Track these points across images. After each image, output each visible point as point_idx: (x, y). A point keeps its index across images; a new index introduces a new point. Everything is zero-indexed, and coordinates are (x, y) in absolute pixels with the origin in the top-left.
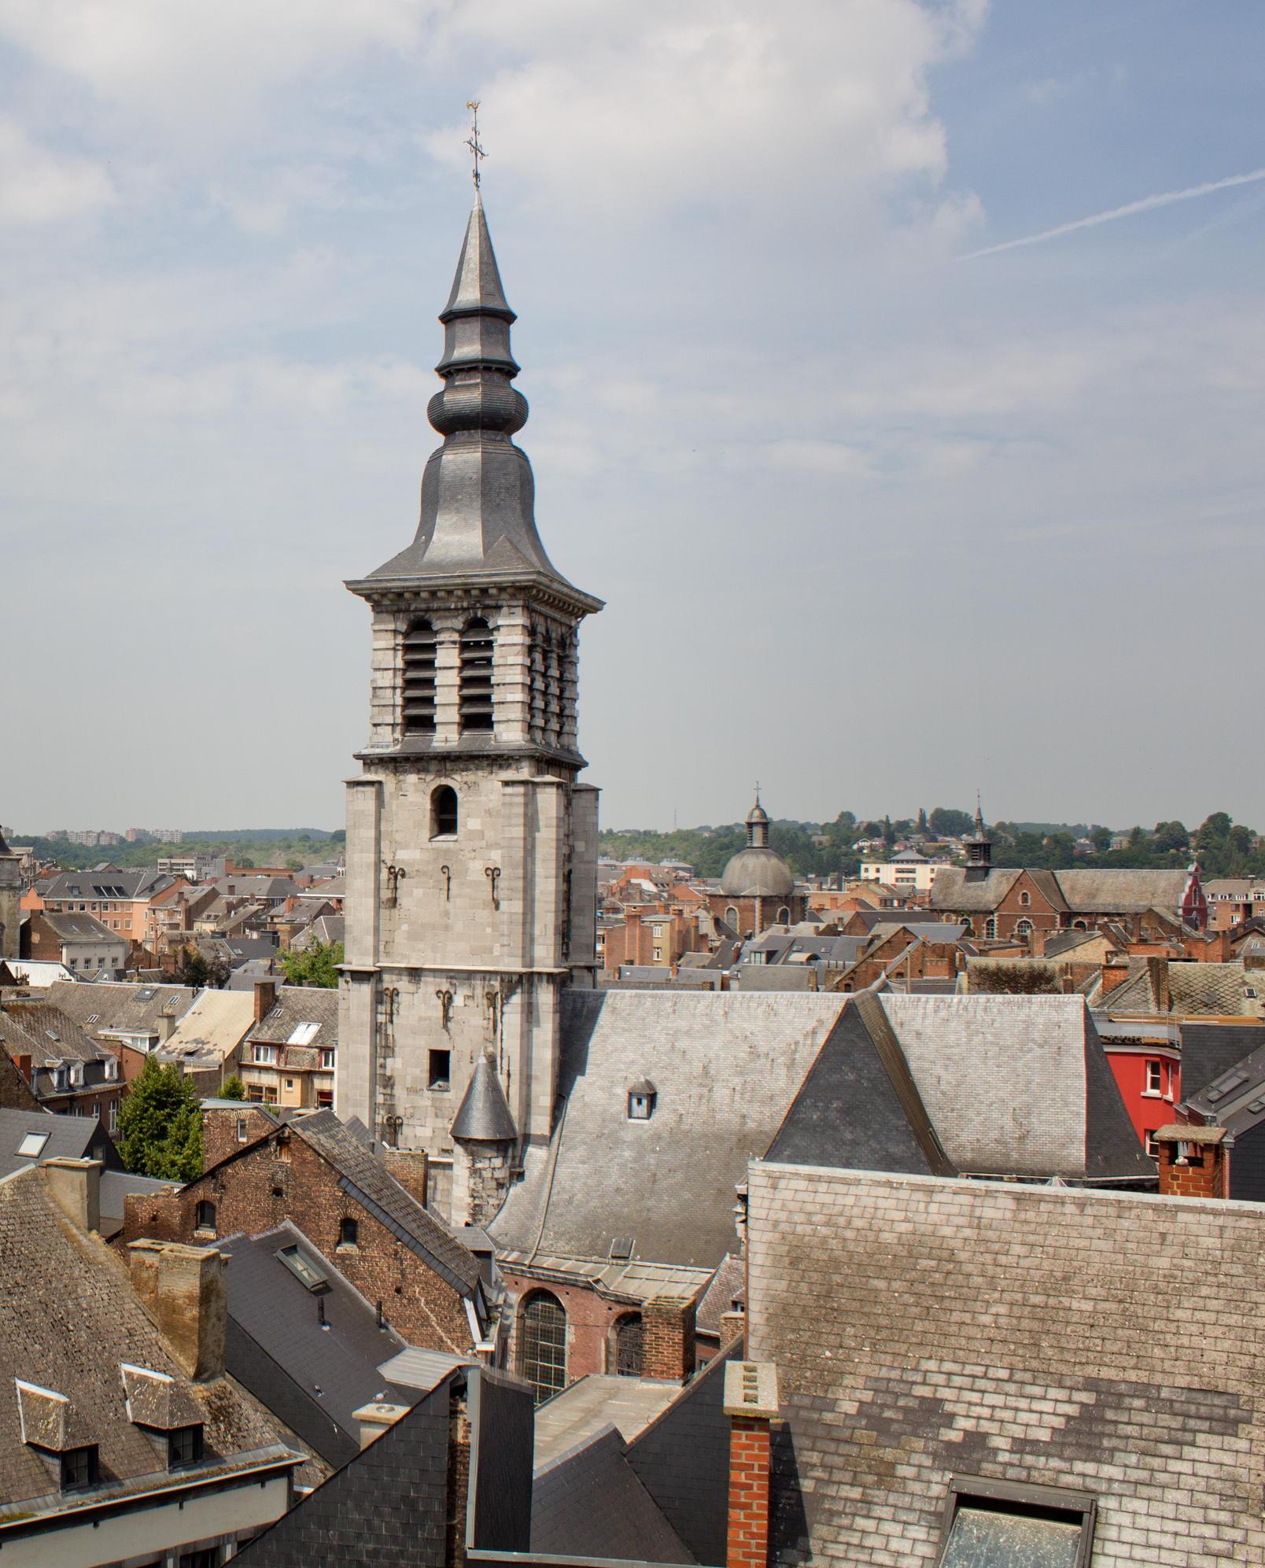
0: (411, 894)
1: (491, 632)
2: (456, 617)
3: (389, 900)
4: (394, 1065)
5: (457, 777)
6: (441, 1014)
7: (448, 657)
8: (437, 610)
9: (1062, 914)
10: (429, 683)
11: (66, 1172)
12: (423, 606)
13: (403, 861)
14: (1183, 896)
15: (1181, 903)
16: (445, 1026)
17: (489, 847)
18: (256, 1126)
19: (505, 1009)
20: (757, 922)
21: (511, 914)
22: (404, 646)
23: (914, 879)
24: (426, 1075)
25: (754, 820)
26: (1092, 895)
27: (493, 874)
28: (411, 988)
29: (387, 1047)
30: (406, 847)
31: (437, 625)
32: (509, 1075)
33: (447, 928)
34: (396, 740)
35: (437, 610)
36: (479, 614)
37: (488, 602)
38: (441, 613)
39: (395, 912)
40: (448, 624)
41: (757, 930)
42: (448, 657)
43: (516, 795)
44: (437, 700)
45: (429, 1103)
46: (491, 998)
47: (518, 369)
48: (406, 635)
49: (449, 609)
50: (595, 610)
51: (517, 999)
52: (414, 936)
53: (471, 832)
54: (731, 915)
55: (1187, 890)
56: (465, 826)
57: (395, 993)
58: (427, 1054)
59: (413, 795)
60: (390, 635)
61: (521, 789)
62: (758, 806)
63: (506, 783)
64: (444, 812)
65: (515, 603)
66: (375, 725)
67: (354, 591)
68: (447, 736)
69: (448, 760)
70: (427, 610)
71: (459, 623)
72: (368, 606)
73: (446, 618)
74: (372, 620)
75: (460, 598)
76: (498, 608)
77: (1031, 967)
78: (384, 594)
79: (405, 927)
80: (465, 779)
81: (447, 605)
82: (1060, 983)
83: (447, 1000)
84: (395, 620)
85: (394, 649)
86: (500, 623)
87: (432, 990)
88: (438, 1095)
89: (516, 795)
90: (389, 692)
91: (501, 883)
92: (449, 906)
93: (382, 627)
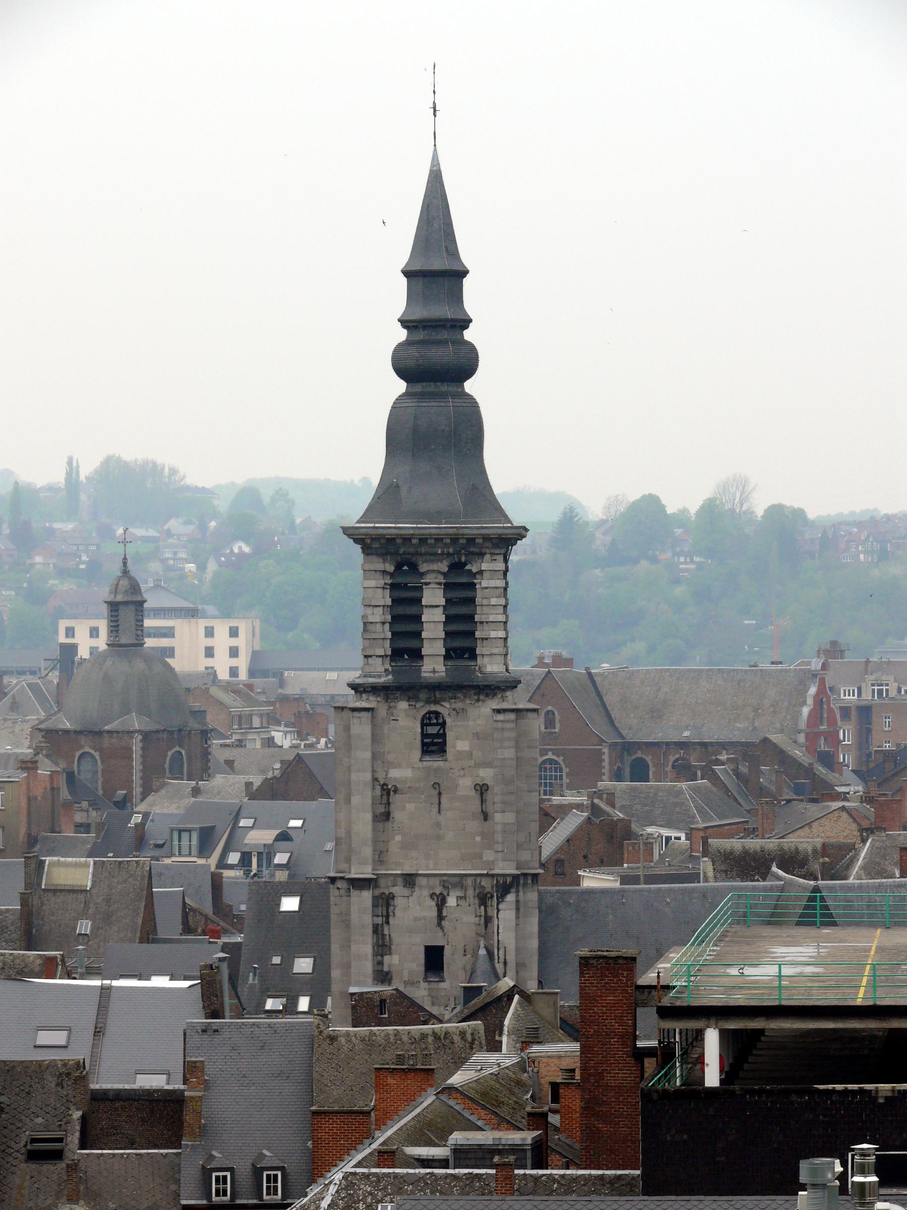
0: (405, 811)
1: (474, 575)
2: (441, 561)
3: (382, 814)
4: (391, 961)
5: (447, 705)
6: (434, 913)
7: (433, 596)
8: (426, 554)
9: (612, 746)
10: (417, 619)
11: (544, 996)
12: (412, 550)
13: (396, 779)
14: (806, 711)
15: (802, 725)
16: (439, 925)
17: (478, 765)
18: (396, 1004)
19: (500, 906)
20: (136, 777)
21: (504, 824)
22: (391, 585)
23: (170, 652)
24: (423, 969)
25: (119, 598)
26: (656, 713)
27: (482, 789)
28: (406, 892)
29: (384, 945)
30: (398, 766)
31: (423, 568)
32: (505, 963)
33: (439, 838)
34: (386, 670)
35: (421, 555)
36: (463, 559)
37: (472, 549)
38: (428, 557)
39: (389, 825)
40: (435, 567)
41: (137, 790)
42: (433, 596)
43: (508, 721)
44: (424, 635)
45: (426, 993)
46: (483, 899)
47: (471, 321)
48: (392, 575)
49: (436, 554)
50: (521, 537)
51: (510, 898)
52: (405, 846)
53: (460, 752)
54: (87, 765)
55: (810, 701)
56: (454, 747)
57: (392, 897)
58: (422, 949)
59: (406, 720)
60: (378, 575)
61: (512, 716)
62: (125, 572)
63: (499, 711)
64: (434, 744)
65: (497, 551)
66: (366, 657)
67: (349, 536)
68: (434, 665)
69: (437, 690)
70: (417, 554)
71: (444, 567)
72: (358, 548)
73: (432, 561)
74: (362, 561)
75: (447, 546)
76: (482, 555)
77: (782, 849)
78: (376, 538)
79: (398, 838)
80: (454, 706)
81: (434, 550)
82: (816, 867)
83: (441, 902)
84: (385, 561)
85: (383, 588)
86: (484, 566)
87: (426, 893)
88: (434, 985)
89: (508, 721)
90: (379, 626)
91: (488, 796)
92: (441, 818)
93: (372, 568)
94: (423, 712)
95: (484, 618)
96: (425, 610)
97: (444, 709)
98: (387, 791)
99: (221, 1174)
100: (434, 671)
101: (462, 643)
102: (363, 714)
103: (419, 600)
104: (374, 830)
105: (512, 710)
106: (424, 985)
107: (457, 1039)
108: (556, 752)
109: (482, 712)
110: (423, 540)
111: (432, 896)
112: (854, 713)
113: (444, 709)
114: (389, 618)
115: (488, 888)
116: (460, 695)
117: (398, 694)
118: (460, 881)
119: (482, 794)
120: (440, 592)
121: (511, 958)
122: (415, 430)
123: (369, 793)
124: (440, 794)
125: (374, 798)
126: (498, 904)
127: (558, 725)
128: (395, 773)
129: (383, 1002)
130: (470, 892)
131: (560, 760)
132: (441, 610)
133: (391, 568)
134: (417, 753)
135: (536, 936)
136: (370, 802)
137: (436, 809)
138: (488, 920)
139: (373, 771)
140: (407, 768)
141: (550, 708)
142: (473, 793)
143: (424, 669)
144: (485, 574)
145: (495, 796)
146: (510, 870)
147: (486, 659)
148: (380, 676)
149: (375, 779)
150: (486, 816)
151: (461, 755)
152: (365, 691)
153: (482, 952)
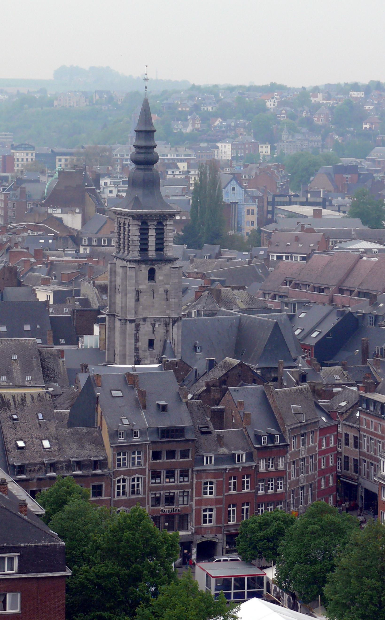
0: (143, 298)
1: (164, 226)
4: (139, 344)
5: (156, 265)
6: (151, 329)
7: (152, 232)
16: (153, 332)
27: (166, 291)
28: (143, 323)
31: (149, 224)
33: (153, 306)
42: (152, 232)
46: (166, 325)
51: (176, 325)
59: (144, 270)
64: (152, 275)
68: (152, 253)
71: (155, 223)
76: (167, 220)
79: (141, 307)
87: (149, 323)
91: (168, 293)
97: (155, 267)
98: (138, 292)
99: (264, 437)
101: (160, 248)
103: (148, 234)
105: (177, 268)
109: (167, 268)
110: (151, 215)
113: (155, 267)
115: (168, 321)
116: (160, 263)
118: (159, 320)
119: (166, 293)
122: (144, 180)
128: (141, 287)
130: (162, 323)
132: (154, 236)
133: (140, 224)
138: (167, 331)
147: (167, 252)
148: (137, 257)
151: (161, 281)
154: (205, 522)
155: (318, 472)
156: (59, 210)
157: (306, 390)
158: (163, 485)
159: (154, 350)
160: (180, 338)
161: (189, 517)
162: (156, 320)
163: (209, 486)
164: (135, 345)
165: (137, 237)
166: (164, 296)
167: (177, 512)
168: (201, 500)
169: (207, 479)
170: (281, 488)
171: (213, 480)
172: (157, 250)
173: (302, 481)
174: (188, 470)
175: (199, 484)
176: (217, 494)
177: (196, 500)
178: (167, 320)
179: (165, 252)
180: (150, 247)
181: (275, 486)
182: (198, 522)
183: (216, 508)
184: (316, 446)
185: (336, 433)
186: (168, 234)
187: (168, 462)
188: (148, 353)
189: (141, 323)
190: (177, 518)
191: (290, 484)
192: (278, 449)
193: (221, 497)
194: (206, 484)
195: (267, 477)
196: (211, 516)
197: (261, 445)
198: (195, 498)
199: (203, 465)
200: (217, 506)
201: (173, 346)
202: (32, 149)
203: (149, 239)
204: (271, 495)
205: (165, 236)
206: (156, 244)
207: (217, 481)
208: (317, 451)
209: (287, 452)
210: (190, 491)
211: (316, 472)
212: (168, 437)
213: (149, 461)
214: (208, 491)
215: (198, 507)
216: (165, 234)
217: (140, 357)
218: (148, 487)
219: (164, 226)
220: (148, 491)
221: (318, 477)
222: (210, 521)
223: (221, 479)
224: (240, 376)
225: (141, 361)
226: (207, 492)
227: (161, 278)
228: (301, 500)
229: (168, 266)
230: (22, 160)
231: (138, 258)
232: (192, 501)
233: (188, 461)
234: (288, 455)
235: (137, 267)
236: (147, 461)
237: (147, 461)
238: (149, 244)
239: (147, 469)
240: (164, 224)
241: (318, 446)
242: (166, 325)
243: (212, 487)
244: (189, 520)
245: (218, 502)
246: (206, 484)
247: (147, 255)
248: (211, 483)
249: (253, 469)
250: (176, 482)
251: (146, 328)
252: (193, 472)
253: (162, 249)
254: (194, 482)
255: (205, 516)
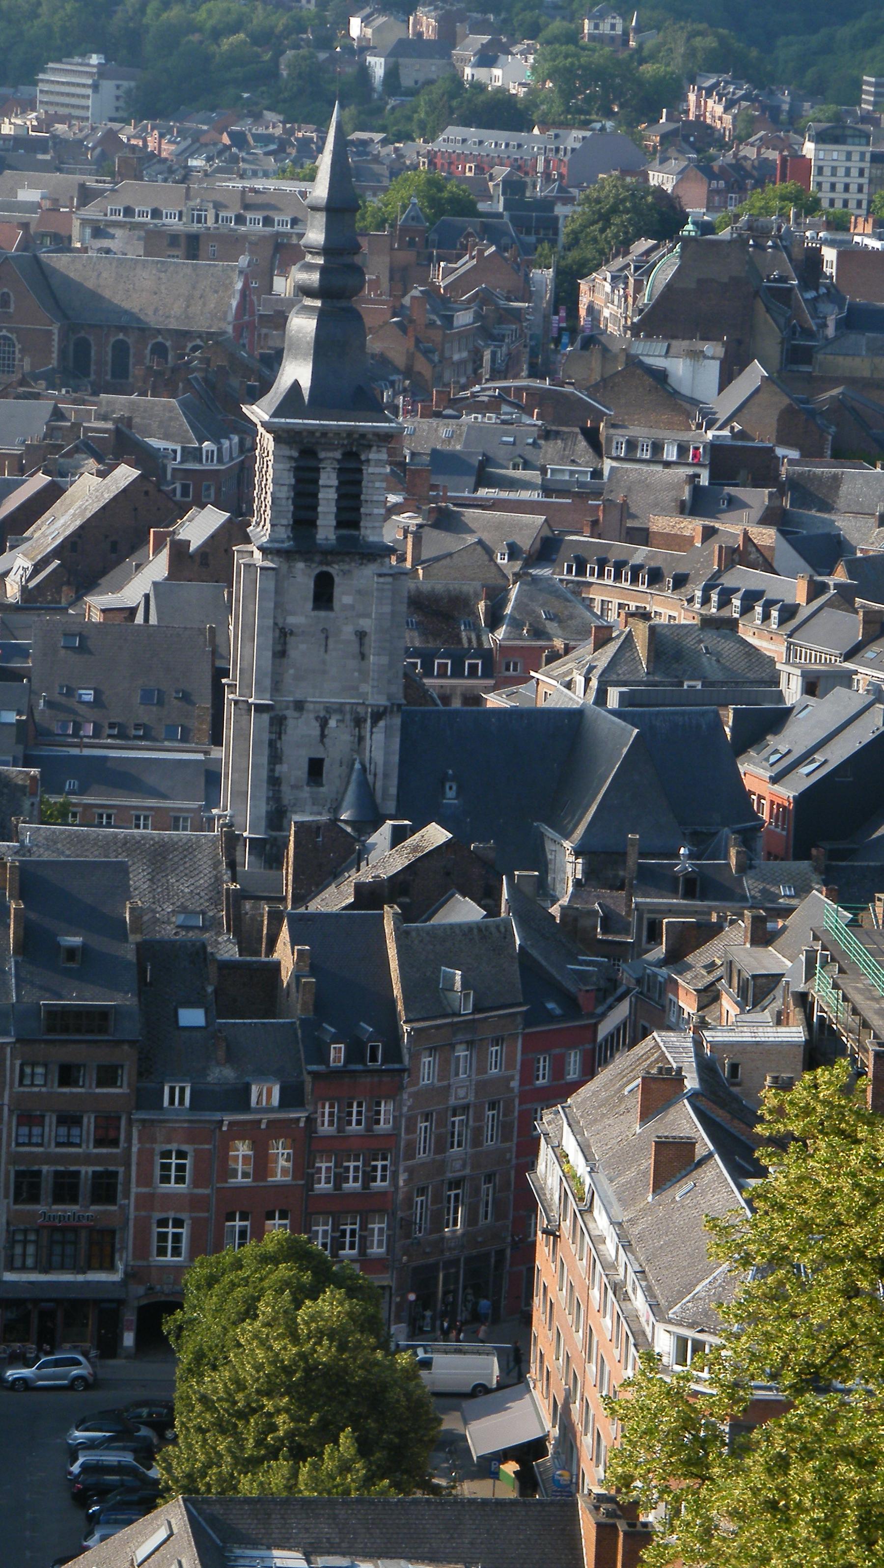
0: (298, 650)
1: (362, 462)
2: (336, 450)
4: (282, 769)
5: (336, 566)
6: (317, 732)
7: (328, 479)
10: (315, 495)
15: (230, 318)
16: (322, 741)
27: (361, 635)
28: (296, 714)
31: (322, 455)
40: (330, 454)
42: (328, 479)
46: (359, 722)
51: (382, 723)
58: (307, 760)
59: (303, 577)
61: (390, 579)
64: (323, 594)
68: (326, 530)
69: (329, 554)
71: (338, 455)
75: (343, 439)
76: (370, 447)
79: (291, 671)
84: (291, 448)
87: (312, 716)
91: (366, 640)
94: (317, 571)
95: (368, 498)
96: (322, 490)
100: (327, 539)
102: (270, 572)
103: (316, 481)
104: (273, 664)
105: (391, 575)
106: (307, 789)
107: (493, 930)
108: (9, 330)
109: (367, 575)
110: (324, 434)
111: (317, 718)
112: (183, 241)
114: (292, 494)
115: (362, 714)
116: (347, 559)
117: (297, 556)
118: (340, 709)
119: (361, 639)
120: (334, 475)
121: (380, 770)
123: (271, 635)
124: (327, 638)
125: (274, 638)
126: (372, 728)
127: (12, 306)
128: (291, 620)
129: (319, 828)
130: (348, 717)
131: (14, 337)
132: (333, 490)
133: (295, 454)
134: (310, 605)
135: (398, 752)
136: (271, 642)
137: (323, 649)
138: (361, 739)
139: (275, 617)
140: (302, 616)
141: (5, 290)
142: (353, 638)
143: (319, 536)
144: (372, 463)
145: (372, 641)
146: (383, 701)
147: (369, 532)
148: (283, 542)
149: (276, 624)
150: (363, 656)
151: (345, 607)
152: (271, 553)
153: (357, 766)
154: (162, 1251)
155: (518, 1145)
156: (660, 347)
157: (500, 932)
158: (50, 1150)
159: (322, 785)
160: (396, 758)
161: (117, 1236)
162: (329, 710)
163: (174, 1161)
164: (272, 771)
165: (285, 488)
166: (355, 648)
167: (85, 1222)
168: (152, 1195)
169: (169, 1142)
170: (383, 1179)
171: (185, 1148)
172: (340, 524)
173: (458, 1165)
174: (119, 1118)
175: (146, 1157)
176: (196, 1184)
177: (137, 1194)
178: (360, 709)
179: (363, 531)
180: (320, 516)
181: (364, 1172)
182: (142, 1251)
183: (192, 1218)
184: (512, 1078)
185: (588, 1046)
186: (370, 485)
187: (65, 1093)
188: (306, 792)
189: (290, 713)
190: (84, 1234)
191: (410, 1171)
192: (376, 1079)
193: (207, 1191)
194: (167, 1154)
195: (340, 1148)
196: (177, 1237)
197: (366, 1065)
198: (134, 1190)
199: (160, 1107)
200: (194, 1215)
201: (370, 778)
202: (863, 141)
203: (320, 496)
204: (353, 1195)
205: (364, 490)
206: (338, 509)
207: (195, 1150)
208: (516, 1090)
209: (400, 1088)
210: (121, 1170)
211: (513, 1144)
212: (66, 1030)
213: (12, 1087)
214: (173, 1173)
215: (143, 1213)
216: (364, 483)
217: (285, 802)
218: (8, 1153)
219: (362, 462)
220: (7, 1163)
221: (517, 1157)
222: (176, 1252)
223: (207, 1147)
224: (448, 874)
225: (286, 811)
226: (169, 1177)
227: (347, 600)
228: (486, 1212)
229: (370, 570)
230: (834, 170)
231: (286, 545)
232: (127, 1196)
233: (117, 1095)
234: (405, 1096)
235: (285, 568)
236: (8, 1087)
237: (8, 1087)
238: (320, 509)
239: (6, 1109)
240: (363, 457)
241: (517, 1077)
242: (359, 722)
243: (185, 1165)
244: (118, 1246)
245: (195, 1203)
246: (167, 1154)
247: (313, 537)
248: (181, 1155)
249: (302, 1124)
250: (84, 1146)
251: (301, 730)
252: (130, 1122)
253: (355, 524)
254: (135, 1149)
255: (163, 1237)
